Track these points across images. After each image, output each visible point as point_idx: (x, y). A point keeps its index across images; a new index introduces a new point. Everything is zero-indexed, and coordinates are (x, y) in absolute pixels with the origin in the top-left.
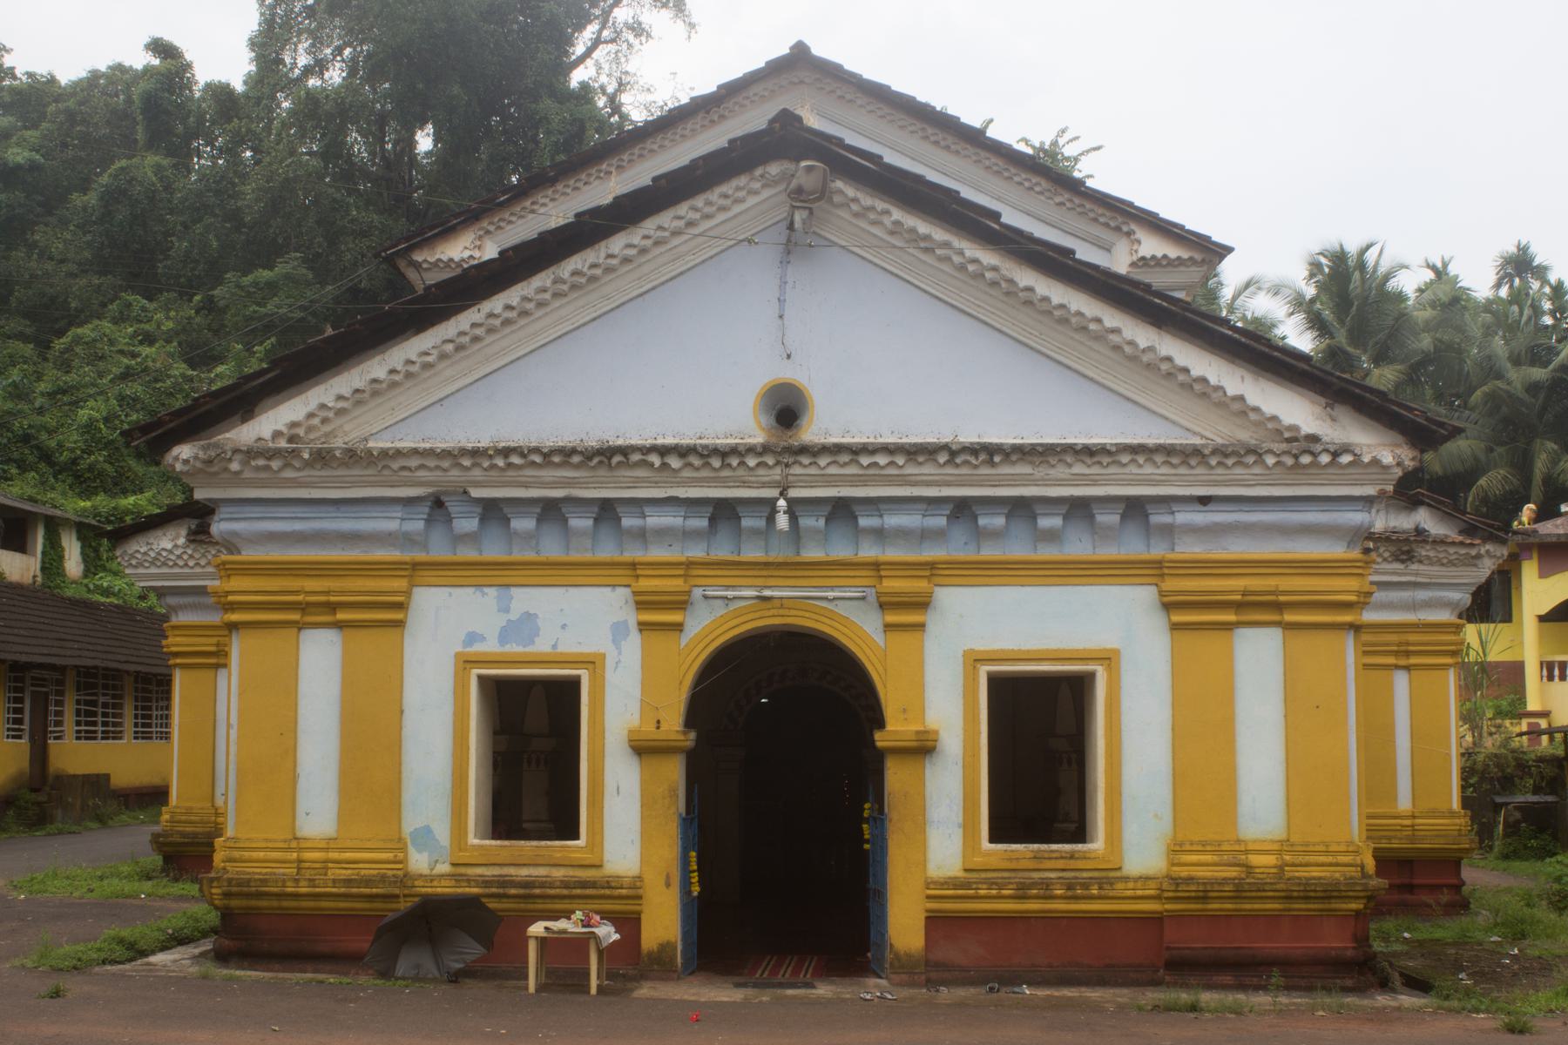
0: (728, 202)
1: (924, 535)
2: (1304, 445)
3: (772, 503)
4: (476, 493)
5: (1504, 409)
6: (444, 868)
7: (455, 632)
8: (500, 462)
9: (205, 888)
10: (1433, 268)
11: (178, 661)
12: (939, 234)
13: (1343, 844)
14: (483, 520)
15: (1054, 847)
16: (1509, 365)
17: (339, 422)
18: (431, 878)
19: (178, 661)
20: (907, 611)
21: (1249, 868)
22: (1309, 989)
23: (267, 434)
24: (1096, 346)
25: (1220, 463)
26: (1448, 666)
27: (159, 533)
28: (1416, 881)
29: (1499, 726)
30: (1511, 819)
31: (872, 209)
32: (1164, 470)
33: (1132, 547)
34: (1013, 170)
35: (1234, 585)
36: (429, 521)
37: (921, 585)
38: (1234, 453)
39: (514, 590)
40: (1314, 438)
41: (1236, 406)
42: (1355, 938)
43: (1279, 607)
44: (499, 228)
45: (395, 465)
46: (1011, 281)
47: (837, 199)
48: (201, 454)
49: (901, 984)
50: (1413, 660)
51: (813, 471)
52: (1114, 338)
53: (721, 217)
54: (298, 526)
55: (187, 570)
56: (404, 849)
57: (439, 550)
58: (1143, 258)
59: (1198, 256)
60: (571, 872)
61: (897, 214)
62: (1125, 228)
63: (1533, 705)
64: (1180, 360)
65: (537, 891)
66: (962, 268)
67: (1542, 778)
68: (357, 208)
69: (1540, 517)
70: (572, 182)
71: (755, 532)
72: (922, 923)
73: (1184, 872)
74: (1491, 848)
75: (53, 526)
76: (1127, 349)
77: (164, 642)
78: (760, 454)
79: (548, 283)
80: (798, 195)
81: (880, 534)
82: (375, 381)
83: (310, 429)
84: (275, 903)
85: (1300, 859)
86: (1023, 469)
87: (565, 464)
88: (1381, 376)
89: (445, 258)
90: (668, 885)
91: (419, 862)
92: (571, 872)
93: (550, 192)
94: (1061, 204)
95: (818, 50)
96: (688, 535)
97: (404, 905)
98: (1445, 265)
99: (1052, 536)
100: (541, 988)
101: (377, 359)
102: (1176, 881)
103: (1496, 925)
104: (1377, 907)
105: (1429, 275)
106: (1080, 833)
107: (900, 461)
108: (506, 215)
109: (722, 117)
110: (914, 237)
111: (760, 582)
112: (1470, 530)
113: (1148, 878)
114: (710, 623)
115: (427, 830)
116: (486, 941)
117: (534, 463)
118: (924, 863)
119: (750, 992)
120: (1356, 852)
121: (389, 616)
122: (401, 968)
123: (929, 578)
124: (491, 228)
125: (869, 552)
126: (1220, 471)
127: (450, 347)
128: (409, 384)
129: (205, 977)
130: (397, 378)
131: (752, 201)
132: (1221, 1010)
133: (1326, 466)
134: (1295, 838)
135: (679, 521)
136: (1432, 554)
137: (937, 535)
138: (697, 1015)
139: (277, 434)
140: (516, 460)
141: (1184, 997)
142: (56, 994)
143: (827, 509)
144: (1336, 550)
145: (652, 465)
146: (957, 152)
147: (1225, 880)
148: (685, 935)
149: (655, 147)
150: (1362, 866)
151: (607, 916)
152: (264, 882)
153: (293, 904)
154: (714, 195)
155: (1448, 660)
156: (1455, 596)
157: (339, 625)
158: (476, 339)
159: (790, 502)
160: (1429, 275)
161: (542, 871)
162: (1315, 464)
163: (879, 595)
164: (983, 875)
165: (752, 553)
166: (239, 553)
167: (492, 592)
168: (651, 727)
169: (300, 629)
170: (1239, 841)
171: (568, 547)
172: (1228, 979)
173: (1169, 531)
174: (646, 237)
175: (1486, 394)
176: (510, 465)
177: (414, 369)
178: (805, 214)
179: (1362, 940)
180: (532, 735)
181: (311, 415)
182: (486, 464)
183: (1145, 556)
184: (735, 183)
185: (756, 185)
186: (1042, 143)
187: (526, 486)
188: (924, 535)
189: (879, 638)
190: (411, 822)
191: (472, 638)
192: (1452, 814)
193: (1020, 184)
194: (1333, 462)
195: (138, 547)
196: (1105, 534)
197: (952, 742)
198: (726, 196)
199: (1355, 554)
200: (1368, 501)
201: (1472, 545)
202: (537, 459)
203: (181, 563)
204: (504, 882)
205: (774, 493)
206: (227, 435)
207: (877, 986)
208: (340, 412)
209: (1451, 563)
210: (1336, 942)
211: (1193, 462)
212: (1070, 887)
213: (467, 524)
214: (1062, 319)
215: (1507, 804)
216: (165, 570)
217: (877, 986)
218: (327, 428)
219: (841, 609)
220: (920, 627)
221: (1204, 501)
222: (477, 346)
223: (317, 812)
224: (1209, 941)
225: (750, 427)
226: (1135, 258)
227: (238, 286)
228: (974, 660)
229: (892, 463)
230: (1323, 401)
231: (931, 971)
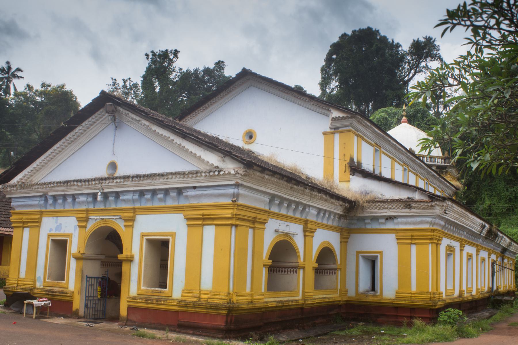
17: (31, 178)
39: (59, 218)
43: (213, 219)
54: (22, 203)
59: (349, 116)
64: (186, 147)
72: (127, 308)
73: (184, 299)
85: (212, 297)
86: (149, 181)
93: (189, 116)
96: (134, 201)
107: (122, 180)
109: (230, 91)
114: (92, 226)
128: (43, 168)
135: (85, 199)
136: (416, 205)
161: (58, 289)
167: (55, 218)
169: (23, 228)
172: (191, 332)
173: (187, 197)
187: (57, 191)
188: (134, 201)
191: (51, 230)
209: (423, 209)
212: (157, 301)
218: (30, 180)
221: (195, 188)
224: (185, 320)
228: (143, 235)
231: (127, 322)
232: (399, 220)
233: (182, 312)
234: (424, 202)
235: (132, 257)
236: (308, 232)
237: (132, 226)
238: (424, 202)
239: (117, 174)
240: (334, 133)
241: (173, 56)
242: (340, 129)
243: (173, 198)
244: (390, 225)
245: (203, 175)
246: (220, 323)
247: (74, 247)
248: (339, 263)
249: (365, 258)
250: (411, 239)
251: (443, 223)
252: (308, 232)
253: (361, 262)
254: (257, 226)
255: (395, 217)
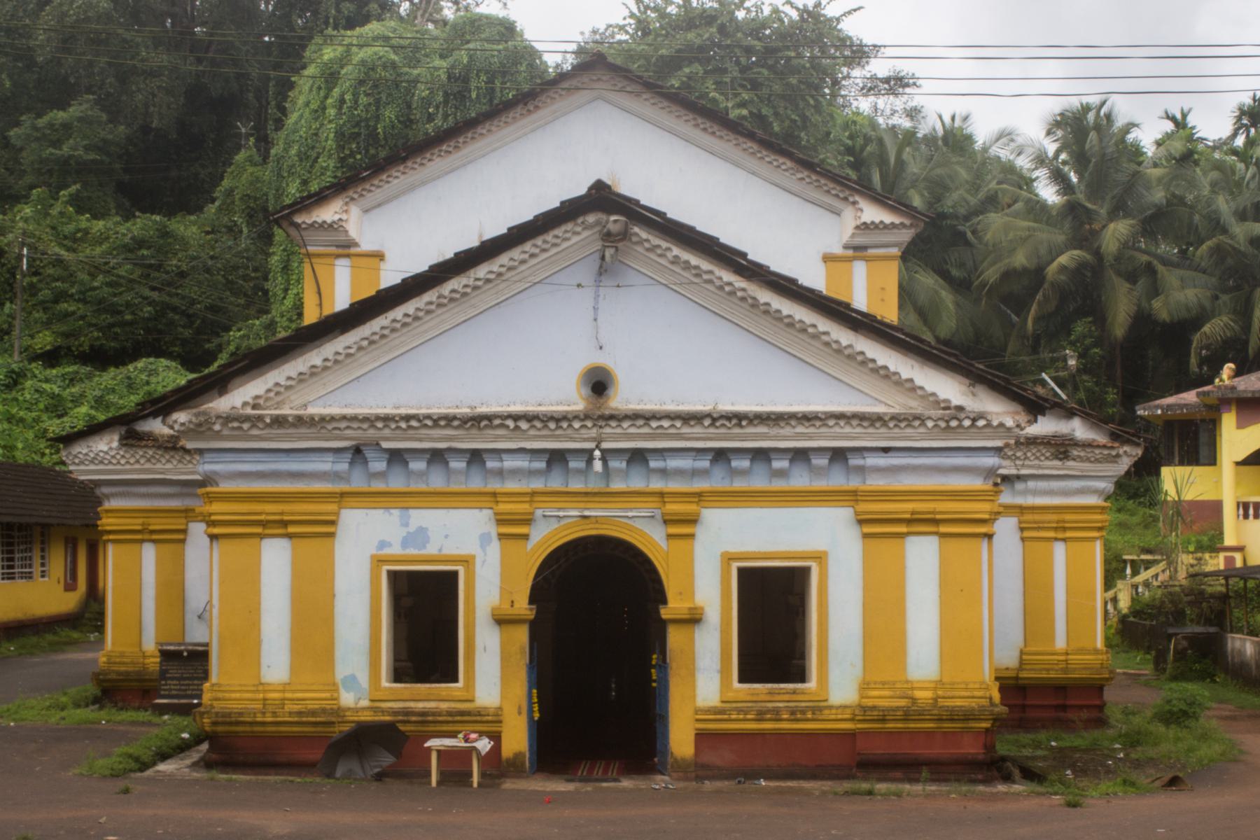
0: (558, 241)
1: (695, 473)
2: (952, 411)
3: (591, 451)
4: (385, 445)
5: (1230, 261)
6: (365, 703)
7: (370, 541)
8: (403, 425)
9: (198, 718)
10: (1173, 119)
11: (111, 537)
12: (705, 265)
13: (978, 686)
14: (390, 462)
15: (782, 686)
16: (1233, 220)
17: (287, 394)
18: (357, 710)
19: (111, 537)
20: (682, 524)
21: (914, 700)
22: (946, 780)
23: (238, 404)
24: (813, 342)
25: (896, 426)
26: (1095, 539)
27: (97, 438)
28: (1068, 703)
29: (1200, 559)
30: (1180, 647)
31: (659, 246)
32: (859, 430)
33: (837, 480)
34: (765, 153)
35: (907, 507)
36: (352, 463)
37: (691, 508)
38: (905, 419)
39: (411, 512)
40: (960, 408)
41: (908, 385)
42: (985, 746)
43: (936, 522)
44: (362, 195)
45: (330, 427)
46: (754, 299)
47: (634, 239)
48: (194, 419)
49: (679, 779)
50: (1069, 534)
51: (619, 431)
52: (825, 338)
53: (554, 250)
55: (119, 467)
56: (337, 690)
57: (358, 482)
58: (865, 223)
59: (907, 222)
60: (453, 705)
61: (676, 251)
62: (851, 199)
63: (1229, 540)
64: (870, 355)
65: (430, 718)
66: (721, 288)
67: (1212, 612)
68: (147, 47)
69: (1238, 373)
70: (419, 160)
71: (579, 471)
72: (692, 738)
73: (869, 703)
74: (1165, 670)
76: (834, 346)
77: (99, 522)
78: (582, 420)
79: (434, 299)
80: (608, 237)
81: (664, 472)
82: (313, 367)
83: (267, 399)
84: (248, 729)
85: (949, 694)
86: (762, 429)
87: (448, 426)
88: (1115, 229)
89: (319, 221)
90: (520, 713)
91: (347, 699)
92: (453, 705)
93: (401, 168)
94: (802, 179)
95: (626, 187)
96: (532, 473)
97: (346, 728)
98: (1184, 116)
99: (782, 474)
100: (439, 783)
101: (315, 351)
102: (864, 709)
103: (1120, 736)
104: (1000, 724)
105: (1169, 126)
106: (801, 677)
107: (678, 424)
108: (367, 187)
109: (537, 107)
110: (687, 266)
111: (582, 505)
112: (1114, 436)
113: (846, 707)
114: (549, 532)
115: (353, 678)
116: (397, 753)
117: (426, 425)
118: (694, 697)
119: (578, 785)
120: (987, 689)
121: (325, 529)
122: (339, 772)
123: (697, 503)
124: (356, 196)
125: (657, 484)
126: (896, 430)
127: (365, 343)
129: (212, 779)
130: (329, 364)
131: (575, 239)
132: (886, 795)
133: (969, 427)
134: (945, 680)
136: (1082, 454)
137: (704, 473)
138: (551, 799)
139: (245, 404)
140: (414, 423)
141: (865, 786)
142: (126, 791)
143: (627, 456)
144: (977, 483)
145: (508, 427)
146: (721, 137)
147: (898, 708)
148: (530, 746)
149: (484, 131)
150: (991, 698)
151: (481, 734)
152: (241, 714)
153: (261, 729)
154: (549, 237)
155: (1095, 534)
156: (1101, 485)
157: (290, 536)
158: (383, 336)
159: (603, 451)
160: (1169, 126)
161: (432, 705)
162: (960, 426)
163: (663, 515)
164: (734, 705)
165: (576, 485)
166: (217, 485)
167: (396, 512)
168: (508, 606)
170: (907, 682)
171: (448, 481)
172: (899, 774)
173: (861, 470)
174: (502, 266)
175: (1210, 248)
176: (410, 427)
177: (340, 358)
178: (612, 251)
179: (990, 748)
180: (424, 614)
181: (269, 391)
182: (393, 426)
183: (846, 488)
184: (563, 228)
185: (579, 229)
186: (805, 6)
187: (420, 440)
188: (532, 473)
189: (663, 544)
190: (341, 672)
191: (383, 544)
192: (1096, 651)
193: (770, 163)
194: (973, 425)
195: (80, 449)
196: (817, 472)
197: (713, 615)
198: (557, 237)
199: (988, 486)
200: (998, 450)
201: (1112, 448)
202: (429, 423)
203: (114, 461)
204: (407, 712)
205: (591, 445)
206: (211, 405)
207: (663, 781)
208: (288, 388)
209: (1097, 461)
210: (972, 749)
211: (878, 425)
212: (793, 713)
213: (379, 465)
214: (790, 323)
215: (1176, 634)
216: (101, 467)
217: (663, 781)
218: (279, 398)
219: (638, 524)
220: (692, 536)
221: (886, 450)
222: (384, 341)
223: (275, 665)
224: (889, 752)
225: (573, 399)
226: (858, 223)
227: (35, 128)
228: (728, 558)
229: (673, 426)
230: (967, 382)
231: (698, 770)
232: (1031, 484)
233: (865, 733)
234: (1098, 447)
238: (1098, 447)
242: (871, 252)
245: (930, 424)
255: (1019, 478)
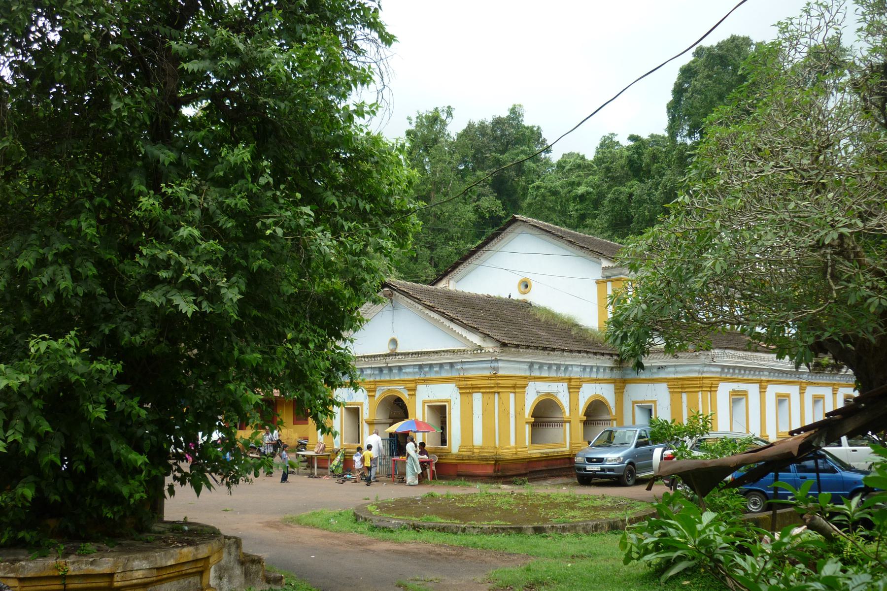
43: (480, 388)
75: (750, 335)
96: (415, 373)
188: (415, 373)
228: (424, 402)
235: (334, 203)
236: (574, 387)
237: (414, 395)
239: (398, 350)
240: (606, 282)
241: (445, 115)
243: (447, 370)
244: (662, 375)
246: (490, 471)
247: (365, 414)
248: (614, 413)
249: (641, 407)
250: (682, 388)
251: (719, 370)
252: (574, 387)
253: (637, 410)
254: (517, 390)
